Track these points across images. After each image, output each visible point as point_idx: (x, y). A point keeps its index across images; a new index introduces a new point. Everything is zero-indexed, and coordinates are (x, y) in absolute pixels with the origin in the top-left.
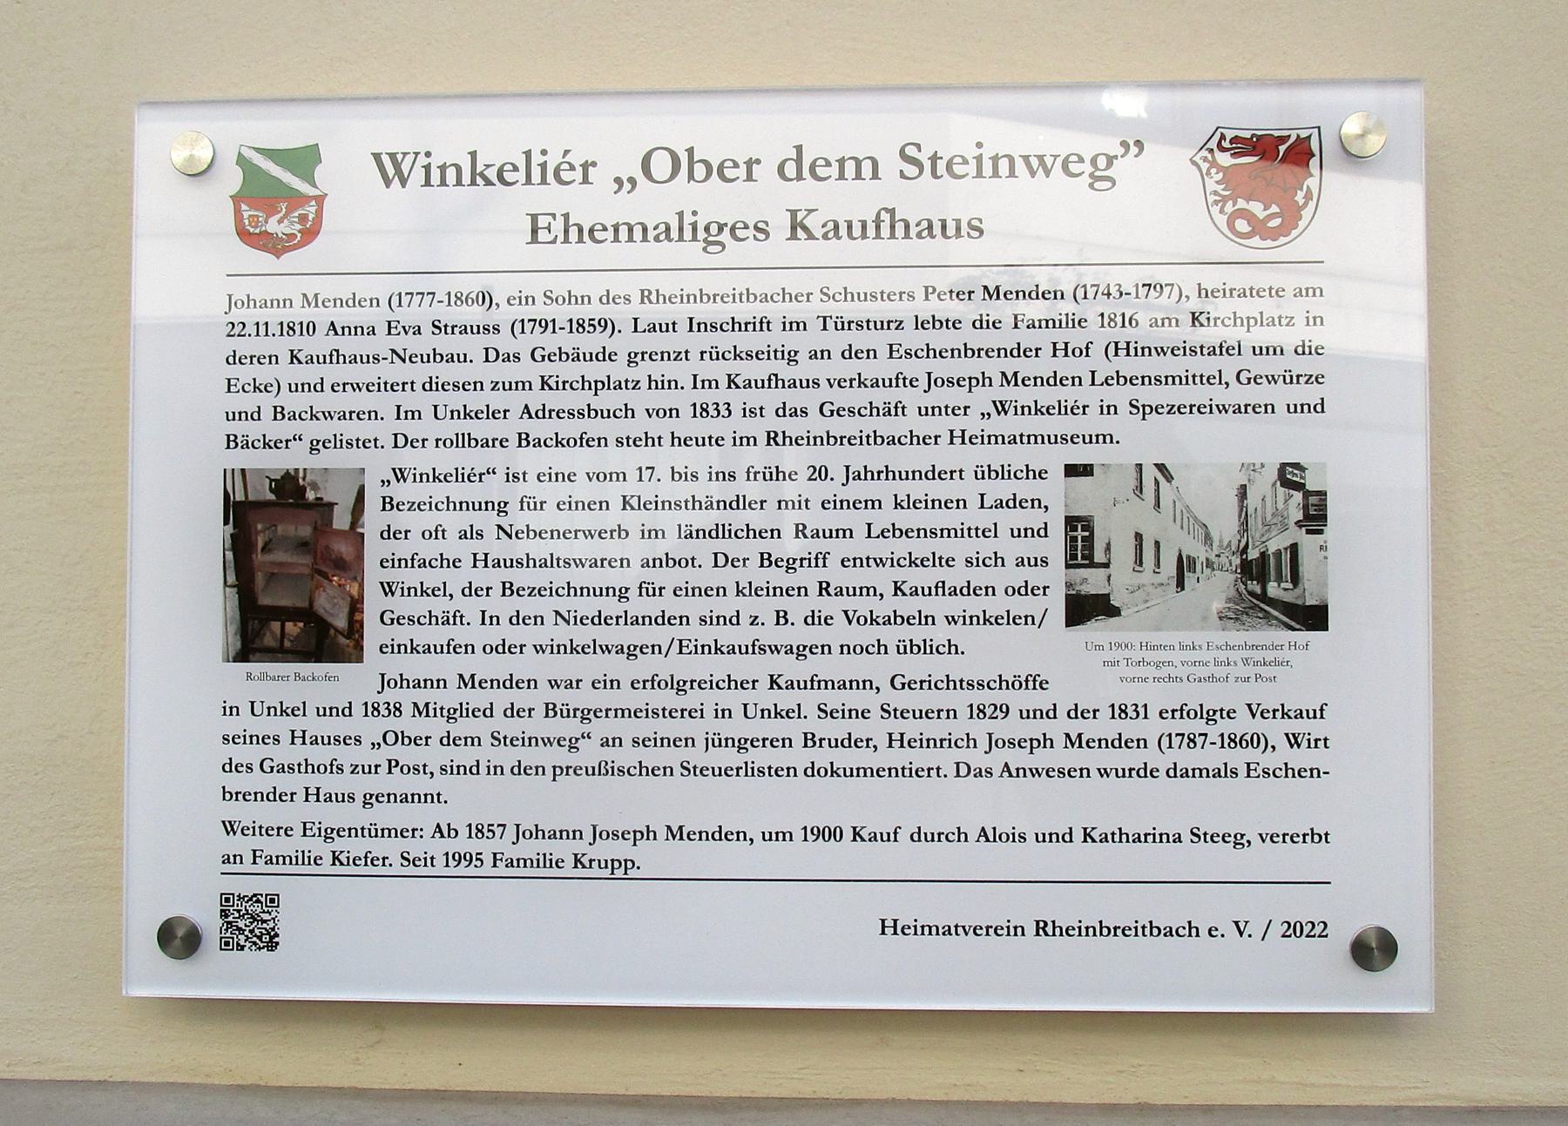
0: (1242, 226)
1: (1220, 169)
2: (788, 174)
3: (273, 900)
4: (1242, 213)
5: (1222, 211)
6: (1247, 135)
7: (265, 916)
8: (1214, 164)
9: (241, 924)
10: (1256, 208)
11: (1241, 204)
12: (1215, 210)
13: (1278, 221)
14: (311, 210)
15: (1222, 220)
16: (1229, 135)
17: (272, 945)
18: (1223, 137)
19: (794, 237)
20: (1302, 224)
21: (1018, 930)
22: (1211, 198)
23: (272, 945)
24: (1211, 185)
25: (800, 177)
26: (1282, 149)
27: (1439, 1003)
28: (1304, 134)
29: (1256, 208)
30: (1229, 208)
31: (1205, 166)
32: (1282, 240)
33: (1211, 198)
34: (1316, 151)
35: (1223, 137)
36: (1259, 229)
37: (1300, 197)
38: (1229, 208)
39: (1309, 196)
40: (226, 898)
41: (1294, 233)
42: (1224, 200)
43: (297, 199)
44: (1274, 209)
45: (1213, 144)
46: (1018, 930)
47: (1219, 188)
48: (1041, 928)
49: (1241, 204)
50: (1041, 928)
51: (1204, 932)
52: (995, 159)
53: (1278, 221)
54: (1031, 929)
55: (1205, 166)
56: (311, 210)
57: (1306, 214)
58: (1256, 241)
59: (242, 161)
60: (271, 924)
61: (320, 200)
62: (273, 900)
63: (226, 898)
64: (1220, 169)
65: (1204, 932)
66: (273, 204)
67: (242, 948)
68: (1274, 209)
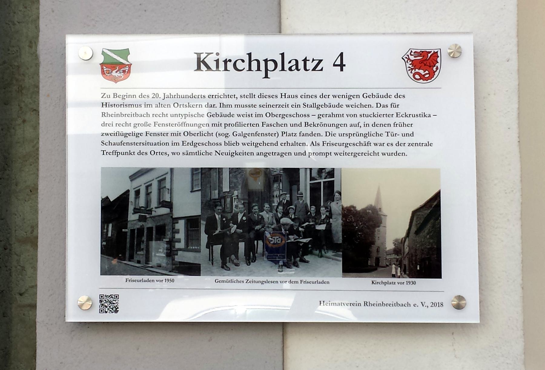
0: (417, 77)
1: (411, 60)
2: (256, 62)
3: (117, 297)
4: (419, 74)
5: (411, 72)
6: (419, 51)
7: (114, 302)
8: (409, 59)
9: (106, 305)
10: (421, 72)
11: (417, 70)
12: (409, 72)
13: (427, 76)
14: (127, 69)
15: (411, 75)
16: (413, 51)
17: (116, 311)
18: (411, 52)
19: (199, 68)
20: (435, 76)
21: (359, 305)
22: (408, 69)
23: (116, 311)
24: (408, 65)
25: (266, 61)
26: (429, 55)
27: (481, 319)
28: (436, 51)
29: (421, 72)
30: (413, 71)
31: (406, 60)
32: (429, 81)
33: (408, 69)
34: (439, 56)
35: (411, 52)
36: (422, 77)
37: (434, 69)
38: (413, 71)
39: (437, 68)
40: (101, 296)
41: (433, 79)
42: (412, 69)
43: (122, 65)
44: (427, 72)
45: (409, 54)
46: (359, 305)
47: (410, 66)
48: (366, 304)
49: (417, 70)
50: (366, 304)
51: (412, 305)
52: (226, 62)
53: (427, 76)
54: (363, 304)
55: (406, 60)
56: (127, 69)
57: (436, 73)
58: (421, 81)
59: (103, 53)
60: (116, 304)
61: (130, 66)
62: (117, 297)
63: (101, 296)
64: (411, 60)
65: (412, 305)
66: (115, 66)
67: (107, 312)
68: (427, 72)
